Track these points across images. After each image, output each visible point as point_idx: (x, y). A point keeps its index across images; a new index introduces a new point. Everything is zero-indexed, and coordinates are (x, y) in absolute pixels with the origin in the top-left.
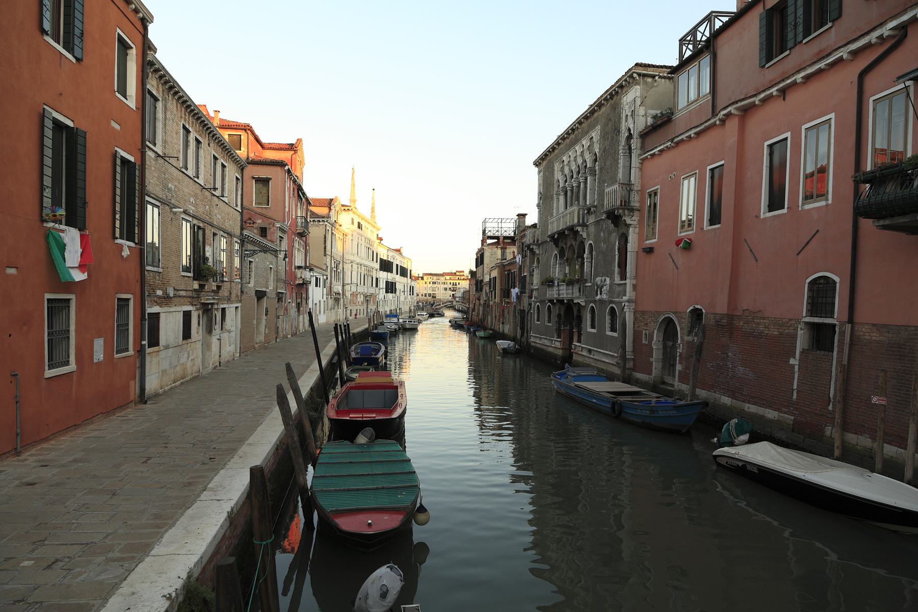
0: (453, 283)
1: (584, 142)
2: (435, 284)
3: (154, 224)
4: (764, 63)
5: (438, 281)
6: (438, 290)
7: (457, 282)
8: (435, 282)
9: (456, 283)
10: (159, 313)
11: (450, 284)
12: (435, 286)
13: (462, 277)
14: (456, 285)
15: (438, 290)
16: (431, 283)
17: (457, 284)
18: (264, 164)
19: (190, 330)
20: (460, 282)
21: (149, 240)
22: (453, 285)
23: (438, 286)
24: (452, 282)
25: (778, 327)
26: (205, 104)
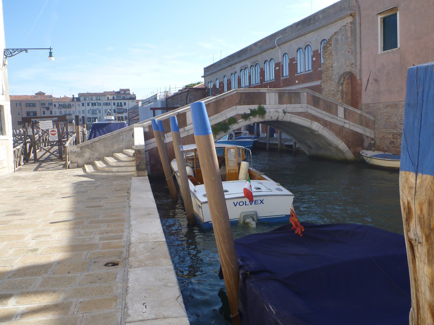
0: (118, 103)
1: (99, 183)
2: (95, 105)
3: (129, 170)
4: (175, 114)
5: (99, 102)
6: (100, 112)
7: (123, 102)
8: (95, 103)
9: (121, 103)
10: (265, 92)
11: (114, 104)
12: (96, 107)
13: (128, 97)
14: (121, 105)
15: (100, 112)
16: (90, 104)
17: (123, 104)
18: (252, 57)
19: (10, 103)
20: (127, 101)
21: (217, 88)
22: (118, 106)
23: (100, 108)
24: (116, 102)
25: (323, 25)
26: (246, 64)
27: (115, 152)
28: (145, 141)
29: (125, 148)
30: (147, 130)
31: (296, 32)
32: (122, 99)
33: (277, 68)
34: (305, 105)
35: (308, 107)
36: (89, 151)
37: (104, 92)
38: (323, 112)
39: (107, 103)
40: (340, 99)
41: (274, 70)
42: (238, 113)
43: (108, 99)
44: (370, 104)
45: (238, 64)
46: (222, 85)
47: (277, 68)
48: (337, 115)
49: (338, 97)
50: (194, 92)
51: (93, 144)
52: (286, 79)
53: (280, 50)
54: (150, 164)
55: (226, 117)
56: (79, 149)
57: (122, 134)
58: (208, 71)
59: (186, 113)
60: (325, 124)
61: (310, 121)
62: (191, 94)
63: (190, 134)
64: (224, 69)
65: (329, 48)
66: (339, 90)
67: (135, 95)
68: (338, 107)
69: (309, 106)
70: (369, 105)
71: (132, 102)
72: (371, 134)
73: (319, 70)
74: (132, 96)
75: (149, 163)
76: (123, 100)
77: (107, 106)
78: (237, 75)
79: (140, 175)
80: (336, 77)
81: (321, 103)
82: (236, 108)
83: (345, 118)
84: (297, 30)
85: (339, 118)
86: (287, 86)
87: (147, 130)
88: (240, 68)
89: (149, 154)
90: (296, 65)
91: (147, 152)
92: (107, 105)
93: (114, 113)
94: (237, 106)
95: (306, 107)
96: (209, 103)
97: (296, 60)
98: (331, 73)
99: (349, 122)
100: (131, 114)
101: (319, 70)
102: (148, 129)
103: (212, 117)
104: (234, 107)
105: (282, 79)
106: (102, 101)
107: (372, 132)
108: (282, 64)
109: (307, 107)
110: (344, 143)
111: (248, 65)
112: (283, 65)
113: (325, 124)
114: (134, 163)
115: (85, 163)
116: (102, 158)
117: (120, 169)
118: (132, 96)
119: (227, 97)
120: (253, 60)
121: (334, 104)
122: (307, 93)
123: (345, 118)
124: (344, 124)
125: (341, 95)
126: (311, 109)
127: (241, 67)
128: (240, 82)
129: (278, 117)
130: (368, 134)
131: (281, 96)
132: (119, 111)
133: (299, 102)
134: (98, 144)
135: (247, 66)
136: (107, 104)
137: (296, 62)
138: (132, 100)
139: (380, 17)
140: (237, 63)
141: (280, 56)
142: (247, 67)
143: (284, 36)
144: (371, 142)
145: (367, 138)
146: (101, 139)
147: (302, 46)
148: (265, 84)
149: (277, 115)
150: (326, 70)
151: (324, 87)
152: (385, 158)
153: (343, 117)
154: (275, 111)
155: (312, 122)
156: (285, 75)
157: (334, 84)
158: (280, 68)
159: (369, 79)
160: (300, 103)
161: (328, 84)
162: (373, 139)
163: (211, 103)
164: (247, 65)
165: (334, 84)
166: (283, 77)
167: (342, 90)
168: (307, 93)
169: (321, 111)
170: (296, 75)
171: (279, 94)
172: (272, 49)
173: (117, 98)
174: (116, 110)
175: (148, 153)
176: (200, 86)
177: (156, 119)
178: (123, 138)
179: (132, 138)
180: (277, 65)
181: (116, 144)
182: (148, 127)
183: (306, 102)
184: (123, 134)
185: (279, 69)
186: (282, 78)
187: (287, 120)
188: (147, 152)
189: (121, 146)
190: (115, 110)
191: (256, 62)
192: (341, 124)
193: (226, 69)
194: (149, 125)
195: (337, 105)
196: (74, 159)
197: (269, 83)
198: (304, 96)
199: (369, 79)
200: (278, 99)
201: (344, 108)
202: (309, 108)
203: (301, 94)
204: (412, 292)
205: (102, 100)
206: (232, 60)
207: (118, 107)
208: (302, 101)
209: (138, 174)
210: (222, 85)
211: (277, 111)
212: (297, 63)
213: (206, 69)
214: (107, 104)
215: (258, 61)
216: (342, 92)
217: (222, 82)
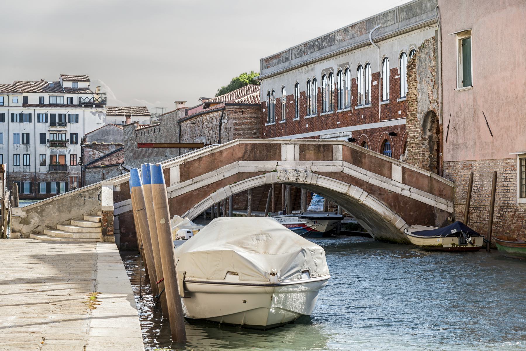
10: (280, 144)
27: (73, 219)
28: (114, 203)
29: (87, 214)
30: (118, 189)
31: (399, 22)
32: (66, 103)
33: (375, 83)
34: (340, 163)
35: (344, 165)
36: (38, 217)
37: (15, 82)
38: (368, 172)
39: (21, 115)
40: (427, 151)
41: (371, 86)
42: (240, 171)
43: (25, 103)
44: (450, 162)
45: (318, 62)
46: (292, 102)
47: (375, 83)
48: (390, 177)
49: (424, 149)
50: (236, 113)
51: (44, 206)
52: (386, 105)
53: (378, 50)
54: (121, 232)
55: (224, 176)
56: (24, 213)
57: (84, 194)
58: (268, 67)
59: (169, 169)
60: (371, 190)
61: (348, 184)
62: (229, 116)
63: (173, 196)
64: (295, 69)
65: (413, 70)
66: (425, 138)
67: (105, 94)
68: (393, 165)
69: (346, 164)
70: (449, 164)
71: (93, 114)
72: (448, 206)
73: (398, 101)
74: (95, 96)
75: (118, 231)
76: (67, 108)
77: (21, 124)
78: (317, 85)
79: (106, 240)
80: (420, 116)
81: (366, 160)
82: (238, 165)
83: (404, 182)
84: (401, 20)
85: (393, 182)
86: (387, 118)
87: (118, 189)
88: (321, 72)
89: (119, 220)
90: (399, 82)
91: (117, 217)
92: (21, 120)
93: (41, 143)
94: (240, 162)
95: (341, 165)
96: (200, 157)
97: (399, 73)
98: (416, 110)
99: (410, 188)
100: (90, 151)
101: (398, 101)
102: (120, 188)
103: (195, 178)
104: (236, 162)
105: (381, 105)
106: (8, 108)
107: (450, 204)
108: (381, 77)
109: (343, 165)
110: (402, 218)
111: (333, 68)
112: (382, 79)
113: (371, 190)
114: (100, 230)
115: (31, 233)
116: (54, 227)
117: (82, 235)
118: (95, 96)
119: (226, 149)
120: (342, 59)
121: (387, 161)
122: (343, 145)
123: (404, 182)
124: (402, 190)
125: (428, 146)
126: (348, 168)
127: (323, 71)
128: (320, 101)
129: (297, 179)
130: (443, 207)
131: (303, 149)
132: (55, 139)
133: (331, 158)
134: (50, 206)
135: (333, 70)
136: (23, 118)
137: (399, 76)
138: (94, 110)
139: (458, 38)
140: (317, 62)
141: (379, 61)
142: (332, 71)
143: (385, 25)
144: (447, 219)
145: (441, 212)
146: (55, 201)
147: (406, 50)
148: (358, 109)
149: (297, 175)
150: (410, 104)
151: (409, 131)
152: (419, 235)
153: (401, 181)
154: (293, 170)
155: (350, 186)
156: (384, 98)
157: (419, 128)
158: (378, 82)
159: (449, 125)
160: (332, 160)
161: (412, 126)
162: (450, 214)
163: (204, 157)
164: (331, 68)
165: (419, 128)
166: (382, 101)
167: (431, 137)
168: (343, 145)
169: (364, 171)
170: (398, 100)
171: (300, 146)
172: (367, 47)
173: (51, 102)
174: (47, 137)
175: (118, 219)
176: (257, 96)
177: (162, 166)
178: (85, 200)
179: (98, 200)
180: (375, 76)
181: (75, 208)
182: (119, 185)
183: (341, 158)
184: (86, 194)
185: (377, 85)
186: (380, 103)
187: (312, 183)
188: (117, 217)
189: (82, 211)
190: (42, 136)
191: (345, 64)
192: (398, 191)
193: (299, 69)
194: (120, 183)
195: (392, 163)
196: (17, 226)
197: (364, 108)
198: (339, 151)
199: (449, 125)
200: (299, 153)
201: (403, 168)
202: (345, 167)
203: (334, 146)
204: (252, 280)
205: (9, 106)
206: (309, 53)
207: (54, 129)
208: (334, 157)
209: (104, 239)
210: (292, 102)
211: (296, 170)
212: (400, 79)
213: (264, 61)
214: (23, 118)
215: (348, 63)
216: (430, 141)
217: (291, 95)
